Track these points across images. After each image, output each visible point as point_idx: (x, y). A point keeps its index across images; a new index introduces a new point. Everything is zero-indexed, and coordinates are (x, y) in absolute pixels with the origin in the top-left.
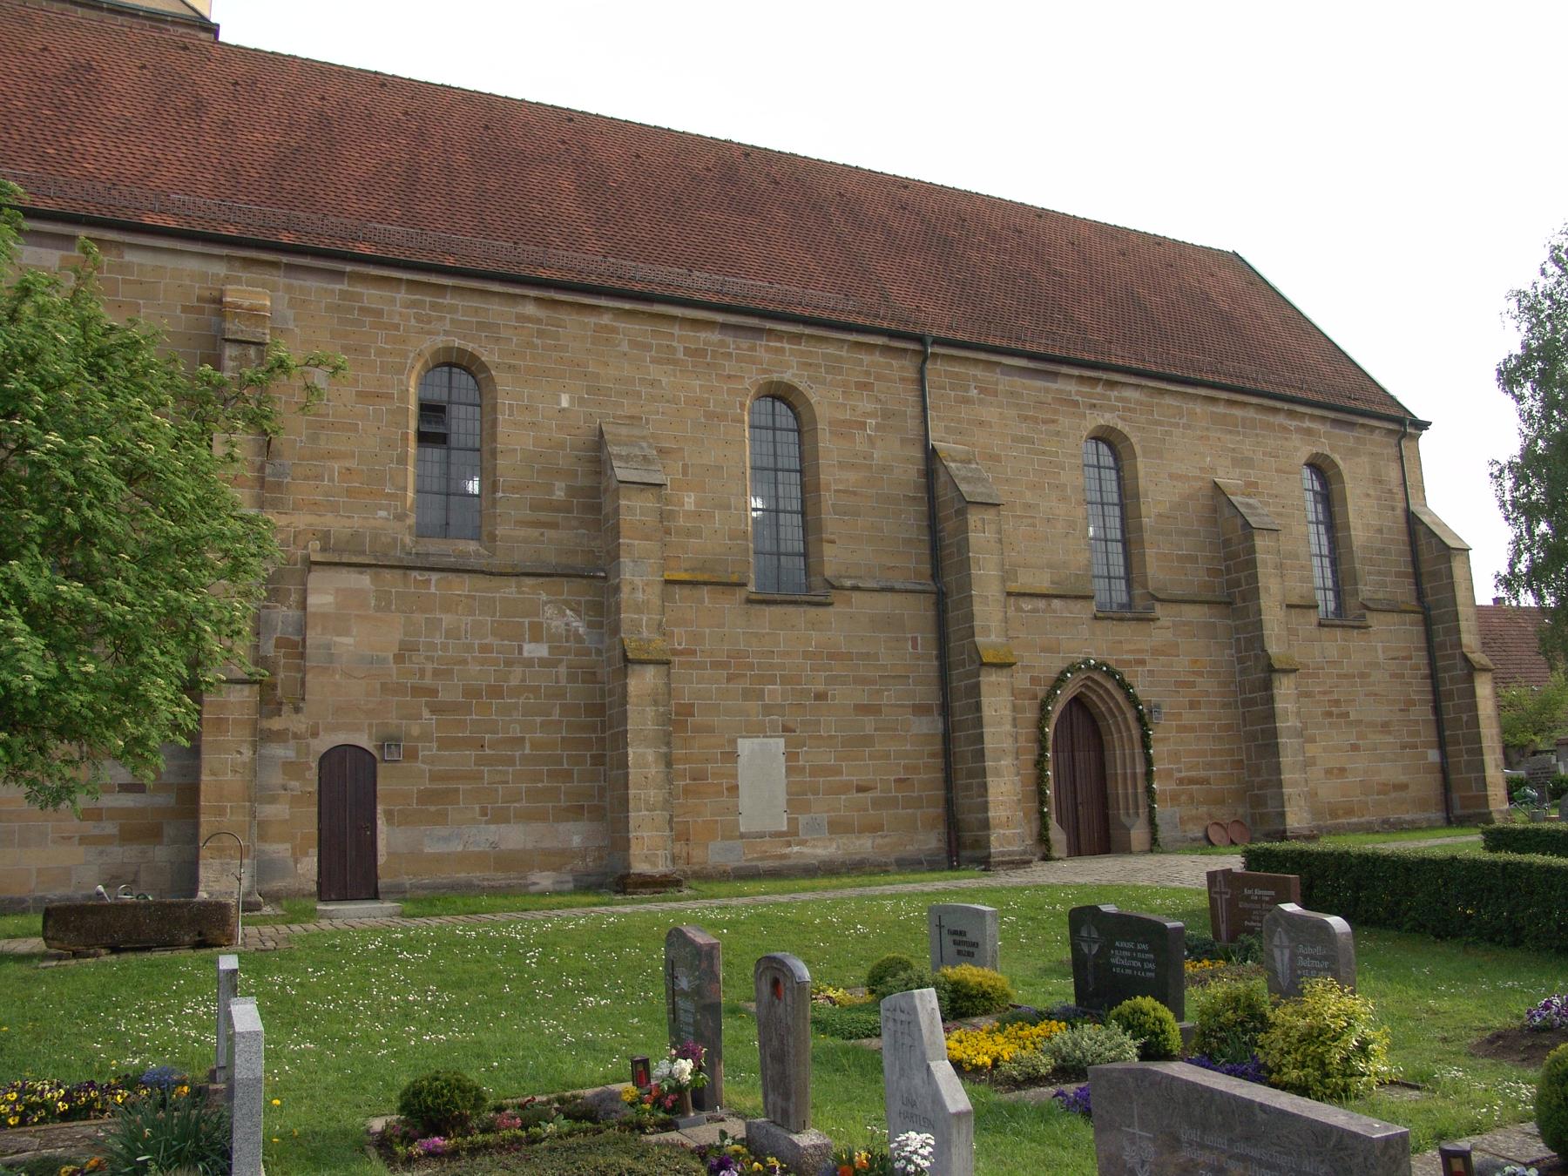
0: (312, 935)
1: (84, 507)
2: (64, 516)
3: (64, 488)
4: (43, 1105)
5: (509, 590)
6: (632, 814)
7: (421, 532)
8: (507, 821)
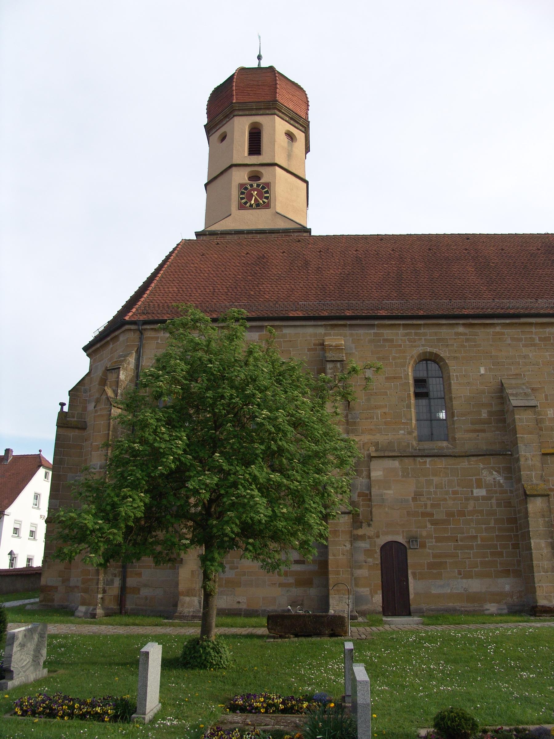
0: (382, 632)
1: (278, 440)
2: (271, 445)
3: (270, 433)
4: (274, 705)
5: (464, 464)
6: (536, 574)
7: (420, 439)
8: (471, 577)
